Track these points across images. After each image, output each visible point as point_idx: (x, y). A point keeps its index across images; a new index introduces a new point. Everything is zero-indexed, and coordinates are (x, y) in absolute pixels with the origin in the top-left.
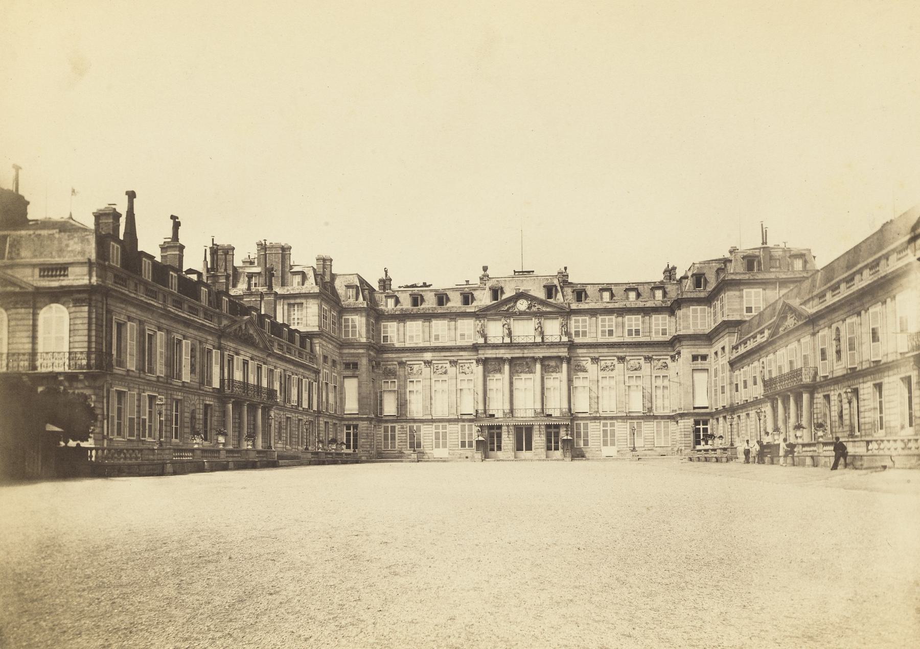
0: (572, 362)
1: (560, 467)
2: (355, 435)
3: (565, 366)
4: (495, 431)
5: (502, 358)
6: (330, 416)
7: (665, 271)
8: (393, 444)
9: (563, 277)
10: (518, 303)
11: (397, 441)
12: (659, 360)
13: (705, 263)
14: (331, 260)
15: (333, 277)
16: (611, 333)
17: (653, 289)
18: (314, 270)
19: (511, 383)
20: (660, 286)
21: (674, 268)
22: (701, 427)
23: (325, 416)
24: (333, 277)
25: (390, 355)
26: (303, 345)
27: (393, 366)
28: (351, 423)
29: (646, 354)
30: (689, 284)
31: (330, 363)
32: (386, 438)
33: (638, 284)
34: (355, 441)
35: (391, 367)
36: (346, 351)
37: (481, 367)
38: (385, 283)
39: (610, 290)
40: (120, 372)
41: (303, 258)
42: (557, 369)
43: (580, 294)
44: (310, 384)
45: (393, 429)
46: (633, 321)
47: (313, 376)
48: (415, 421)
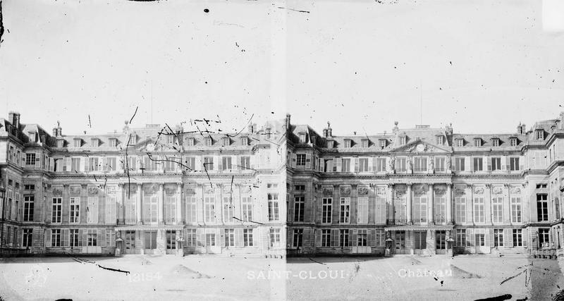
0: (454, 187)
6: (11, 223)
7: (519, 127)
10: (418, 146)
11: (339, 242)
12: (514, 187)
13: (544, 122)
14: (19, 115)
21: (524, 126)
22: (499, 233)
23: (7, 222)
24: (21, 127)
28: (298, 228)
29: (486, 183)
30: (533, 135)
31: (14, 185)
33: (500, 135)
35: (329, 189)
36: (297, 177)
38: (521, 128)
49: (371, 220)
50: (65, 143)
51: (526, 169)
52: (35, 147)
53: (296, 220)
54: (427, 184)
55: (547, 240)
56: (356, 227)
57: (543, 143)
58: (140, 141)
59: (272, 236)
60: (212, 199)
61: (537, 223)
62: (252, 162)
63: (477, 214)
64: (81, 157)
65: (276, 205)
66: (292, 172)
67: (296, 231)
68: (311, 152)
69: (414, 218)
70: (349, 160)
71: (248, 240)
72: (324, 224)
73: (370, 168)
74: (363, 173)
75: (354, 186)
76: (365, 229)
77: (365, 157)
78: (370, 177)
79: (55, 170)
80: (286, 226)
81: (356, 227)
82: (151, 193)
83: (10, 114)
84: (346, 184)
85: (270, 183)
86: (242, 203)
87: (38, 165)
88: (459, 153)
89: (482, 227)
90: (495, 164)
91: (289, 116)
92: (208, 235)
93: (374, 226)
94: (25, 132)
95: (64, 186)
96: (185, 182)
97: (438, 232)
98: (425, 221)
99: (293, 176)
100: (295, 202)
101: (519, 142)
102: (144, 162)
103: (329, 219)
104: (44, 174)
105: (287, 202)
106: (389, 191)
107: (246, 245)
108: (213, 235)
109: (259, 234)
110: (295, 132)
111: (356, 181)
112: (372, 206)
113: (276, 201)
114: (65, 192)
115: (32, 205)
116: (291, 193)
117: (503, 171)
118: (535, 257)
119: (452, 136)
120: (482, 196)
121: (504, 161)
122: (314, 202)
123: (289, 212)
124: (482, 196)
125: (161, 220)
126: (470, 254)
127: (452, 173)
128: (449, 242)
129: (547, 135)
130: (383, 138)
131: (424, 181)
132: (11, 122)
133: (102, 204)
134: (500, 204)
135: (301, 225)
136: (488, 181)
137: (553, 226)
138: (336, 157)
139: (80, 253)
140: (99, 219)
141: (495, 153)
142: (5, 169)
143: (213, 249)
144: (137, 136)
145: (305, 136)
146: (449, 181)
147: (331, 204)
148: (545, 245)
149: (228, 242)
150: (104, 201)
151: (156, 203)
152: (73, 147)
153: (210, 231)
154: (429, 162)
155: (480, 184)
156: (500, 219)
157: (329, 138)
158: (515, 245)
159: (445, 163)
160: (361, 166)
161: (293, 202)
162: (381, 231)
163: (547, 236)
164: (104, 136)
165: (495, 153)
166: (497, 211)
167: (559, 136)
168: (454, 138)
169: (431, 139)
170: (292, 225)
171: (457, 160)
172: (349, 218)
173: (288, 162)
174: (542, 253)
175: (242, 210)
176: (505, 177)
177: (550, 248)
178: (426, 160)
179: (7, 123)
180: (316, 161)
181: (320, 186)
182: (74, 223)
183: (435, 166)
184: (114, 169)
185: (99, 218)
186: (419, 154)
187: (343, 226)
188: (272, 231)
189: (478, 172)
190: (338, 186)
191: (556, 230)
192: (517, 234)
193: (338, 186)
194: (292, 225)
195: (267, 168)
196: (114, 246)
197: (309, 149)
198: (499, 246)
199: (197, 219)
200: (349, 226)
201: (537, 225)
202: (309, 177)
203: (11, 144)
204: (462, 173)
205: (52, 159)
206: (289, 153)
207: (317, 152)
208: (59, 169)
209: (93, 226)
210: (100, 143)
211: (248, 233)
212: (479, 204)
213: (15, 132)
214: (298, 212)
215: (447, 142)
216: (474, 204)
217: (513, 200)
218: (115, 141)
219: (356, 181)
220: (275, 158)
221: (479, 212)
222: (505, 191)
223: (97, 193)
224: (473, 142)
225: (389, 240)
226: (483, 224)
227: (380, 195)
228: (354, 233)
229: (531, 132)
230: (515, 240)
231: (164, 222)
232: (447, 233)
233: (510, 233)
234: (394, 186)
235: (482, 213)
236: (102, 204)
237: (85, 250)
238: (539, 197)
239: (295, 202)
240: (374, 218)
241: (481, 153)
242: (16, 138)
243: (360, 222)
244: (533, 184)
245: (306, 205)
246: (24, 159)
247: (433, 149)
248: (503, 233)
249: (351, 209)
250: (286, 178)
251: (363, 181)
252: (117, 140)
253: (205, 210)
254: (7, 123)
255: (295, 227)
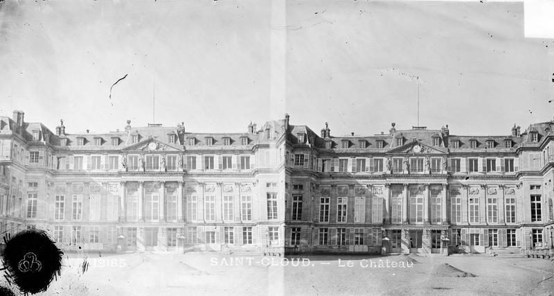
0: (450, 188)
2: (326, 235)
5: (137, 182)
7: (513, 129)
10: (150, 144)
13: (538, 124)
14: (23, 114)
15: (25, 125)
24: (25, 125)
25: (60, 178)
28: (296, 226)
34: (326, 239)
37: (388, 190)
49: (368, 219)
50: (68, 142)
51: (519, 170)
52: (39, 145)
53: (294, 219)
54: (423, 184)
55: (540, 240)
56: (354, 226)
57: (537, 145)
58: (141, 140)
59: (271, 234)
60: (212, 198)
61: (531, 223)
62: (516, 164)
63: (472, 214)
64: (349, 158)
65: (275, 203)
66: (291, 172)
67: (294, 230)
68: (309, 152)
69: (411, 217)
70: (347, 160)
71: (511, 241)
72: (322, 223)
73: (367, 168)
74: (96, 171)
75: (352, 186)
76: (361, 228)
77: (363, 158)
78: (366, 178)
79: (58, 168)
80: (284, 224)
81: (354, 226)
82: (417, 193)
83: (14, 113)
84: (343, 184)
85: (268, 182)
86: (506, 204)
87: (307, 166)
88: (455, 154)
89: (477, 227)
90: (490, 165)
91: (288, 117)
92: (472, 235)
93: (105, 223)
94: (29, 130)
95: (332, 186)
96: (450, 183)
97: (433, 231)
98: (157, 219)
99: (291, 175)
100: (293, 201)
101: (249, 141)
102: (145, 160)
103: (327, 218)
104: (312, 174)
105: (286, 201)
106: (121, 189)
107: (245, 242)
108: (477, 235)
109: (258, 233)
110: (294, 133)
111: (88, 179)
112: (369, 206)
113: (275, 200)
114: (333, 192)
115: (300, 204)
116: (290, 193)
117: (234, 170)
118: (529, 256)
119: (447, 137)
120: (213, 194)
121: (499, 162)
122: (313, 203)
123: (287, 211)
124: (213, 194)
125: (427, 220)
126: (465, 253)
127: (184, 171)
128: (445, 242)
129: (542, 136)
130: (115, 136)
131: (420, 181)
132: (16, 121)
133: (369, 204)
134: (230, 202)
135: (299, 224)
136: (238, 180)
137: (546, 227)
138: (69, 155)
139: (347, 251)
140: (366, 219)
141: (489, 154)
142: (9, 167)
143: (477, 248)
144: (139, 135)
145: (38, 134)
146: (180, 179)
147: (329, 204)
148: (538, 244)
149: (491, 242)
150: (371, 201)
151: (157, 202)
152: (341, 149)
153: (475, 231)
154: (425, 163)
155: (211, 182)
156: (495, 219)
157: (62, 135)
158: (509, 245)
159: (177, 161)
160: (94, 164)
161: (290, 201)
162: (112, 228)
163: (540, 236)
164: (106, 135)
165: (489, 154)
166: (492, 212)
167: (551, 138)
168: (185, 137)
169: (428, 140)
170: (290, 224)
171: (453, 160)
172: (81, 215)
173: (287, 161)
174: (535, 253)
175: (242, 209)
176: (237, 175)
177: (543, 248)
178: (158, 158)
179: (11, 121)
180: (314, 160)
181: (317, 186)
182: (77, 220)
183: (167, 164)
184: (381, 170)
185: (366, 217)
186: (151, 152)
187: (341, 225)
188: (271, 229)
189: (209, 171)
190: (354, 185)
191: (549, 231)
192: (511, 233)
193: (336, 186)
194: (290, 224)
195: (529, 170)
196: (116, 242)
197: (308, 152)
198: (493, 246)
199: (463, 220)
200: (345, 225)
201: (531, 225)
202: (306, 177)
203: (15, 142)
204: (456, 174)
205: (55, 157)
206: (288, 153)
207: (315, 152)
208: (63, 167)
209: (360, 225)
210: (103, 141)
211: (247, 231)
212: (210, 202)
213: (20, 131)
214: (296, 212)
215: (178, 141)
216: (469, 204)
217: (508, 200)
218: (117, 139)
219: (353, 181)
220: (275, 157)
221: (474, 212)
222: (236, 189)
223: (99, 191)
224: (204, 141)
225: (380, 241)
226: (478, 224)
227: (377, 195)
228: (351, 232)
229: (262, 131)
230: (509, 240)
231: (430, 221)
232: (443, 233)
233: (504, 233)
234: (126, 183)
235: (477, 213)
236: (369, 204)
237: (351, 249)
238: (532, 198)
239: (293, 201)
240: (371, 218)
241: (213, 152)
242: (20, 136)
243: (357, 221)
244: (526, 185)
245: (304, 205)
246: (27, 157)
247: (165, 148)
248: (234, 231)
249: (349, 208)
250: (284, 177)
251: (360, 181)
252: (119, 139)
253: (205, 208)
254: (11, 121)
255: (293, 226)
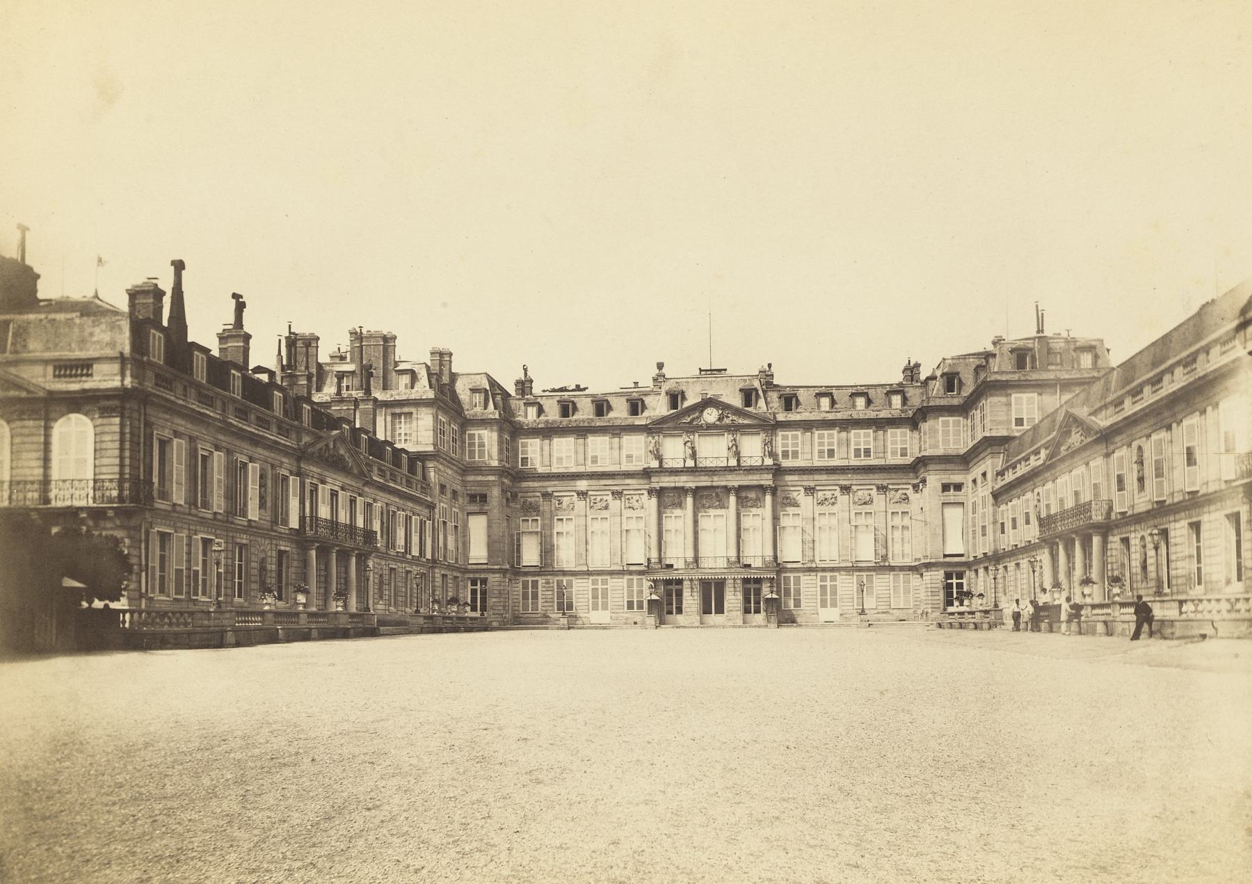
0: (779, 493)
1: (762, 636)
2: (484, 593)
3: (768, 498)
4: (674, 587)
5: (683, 488)
6: (449, 567)
7: (905, 370)
8: (535, 604)
9: (767, 377)
10: (705, 413)
11: (540, 601)
12: (897, 490)
13: (959, 358)
14: (451, 354)
15: (454, 377)
16: (831, 453)
17: (888, 394)
18: (428, 367)
19: (696, 522)
20: (899, 390)
21: (917, 366)
22: (954, 581)
23: (442, 566)
24: (454, 377)
25: (531, 484)
26: (412, 470)
27: (535, 498)
28: (477, 576)
29: (879, 482)
30: (937, 387)
31: (449, 495)
32: (525, 597)
33: (869, 386)
34: (484, 600)
35: (533, 500)
36: (471, 478)
37: (654, 500)
38: (524, 386)
39: (830, 395)
40: (163, 507)
41: (412, 351)
42: (758, 503)
43: (790, 401)
44: (422, 524)
45: (535, 584)
46: (861, 438)
47: (426, 512)
48: (564, 573)
